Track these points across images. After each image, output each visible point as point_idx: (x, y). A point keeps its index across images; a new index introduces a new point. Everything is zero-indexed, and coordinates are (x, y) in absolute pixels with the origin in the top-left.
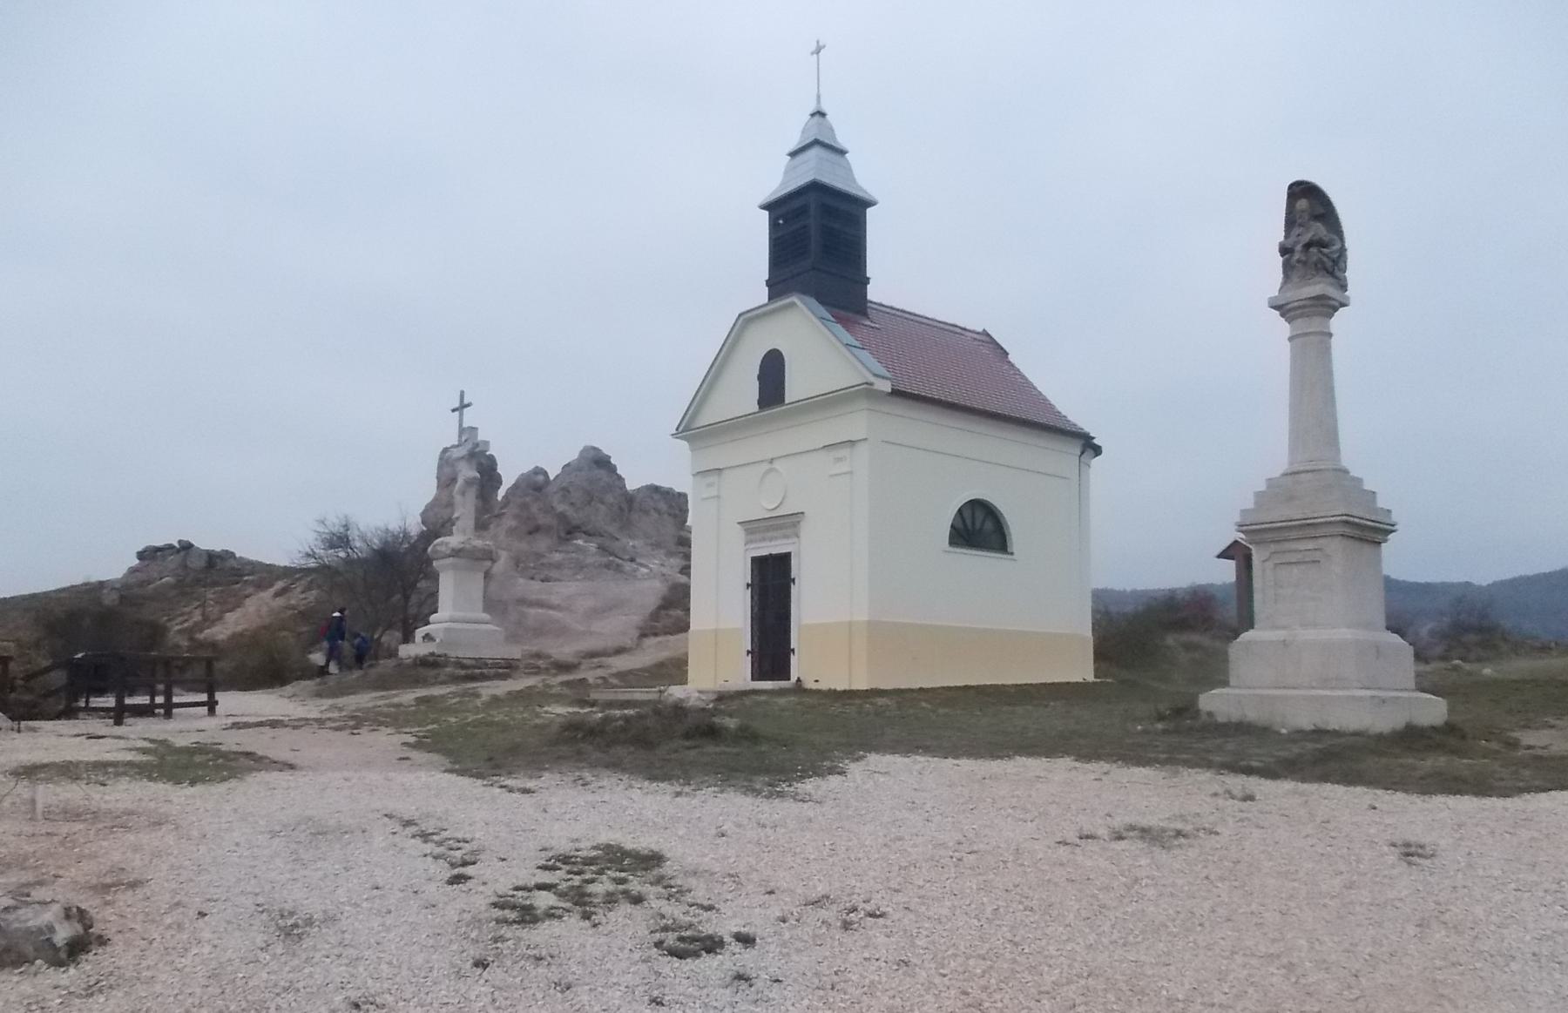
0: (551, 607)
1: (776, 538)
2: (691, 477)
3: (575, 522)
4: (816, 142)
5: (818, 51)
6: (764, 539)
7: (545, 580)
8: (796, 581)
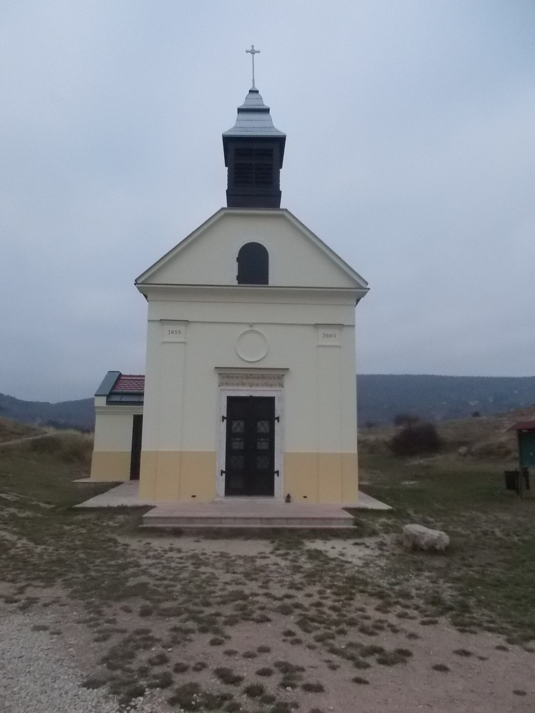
2: (147, 321)
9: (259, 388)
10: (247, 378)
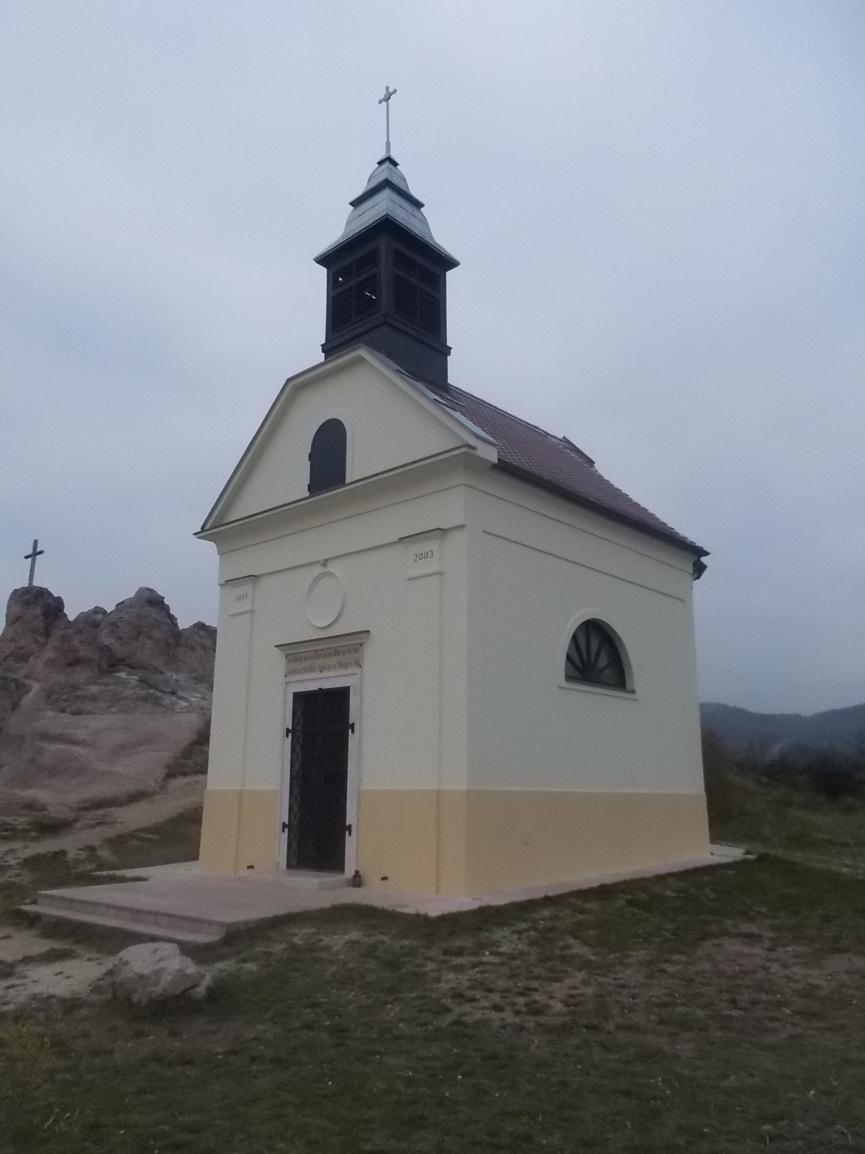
0: (75, 743)
1: (329, 668)
3: (120, 655)
5: (387, 98)
6: (312, 669)
7: (78, 713)
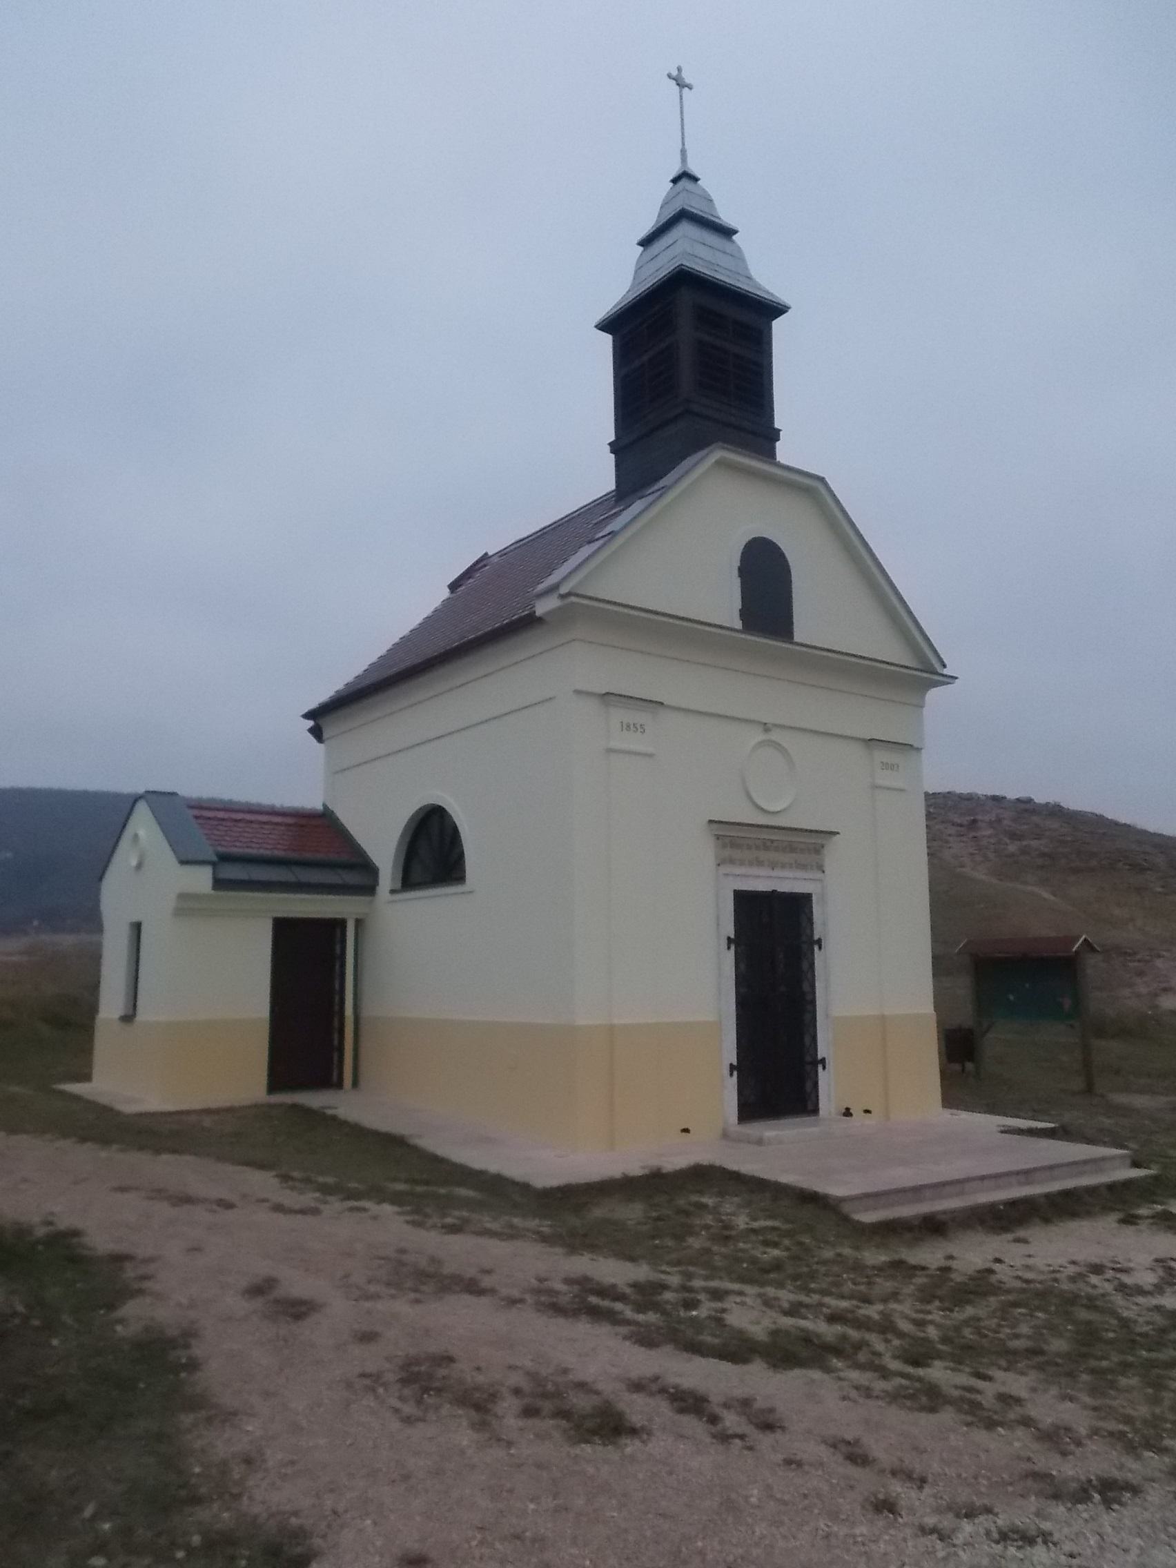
1: (783, 866)
4: (683, 216)
6: (760, 863)
8: (724, 943)
9: (787, 873)
10: (766, 848)
